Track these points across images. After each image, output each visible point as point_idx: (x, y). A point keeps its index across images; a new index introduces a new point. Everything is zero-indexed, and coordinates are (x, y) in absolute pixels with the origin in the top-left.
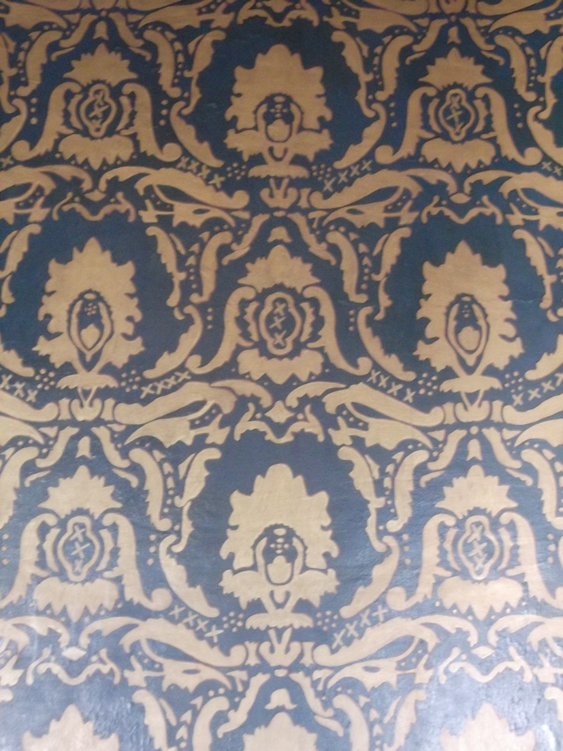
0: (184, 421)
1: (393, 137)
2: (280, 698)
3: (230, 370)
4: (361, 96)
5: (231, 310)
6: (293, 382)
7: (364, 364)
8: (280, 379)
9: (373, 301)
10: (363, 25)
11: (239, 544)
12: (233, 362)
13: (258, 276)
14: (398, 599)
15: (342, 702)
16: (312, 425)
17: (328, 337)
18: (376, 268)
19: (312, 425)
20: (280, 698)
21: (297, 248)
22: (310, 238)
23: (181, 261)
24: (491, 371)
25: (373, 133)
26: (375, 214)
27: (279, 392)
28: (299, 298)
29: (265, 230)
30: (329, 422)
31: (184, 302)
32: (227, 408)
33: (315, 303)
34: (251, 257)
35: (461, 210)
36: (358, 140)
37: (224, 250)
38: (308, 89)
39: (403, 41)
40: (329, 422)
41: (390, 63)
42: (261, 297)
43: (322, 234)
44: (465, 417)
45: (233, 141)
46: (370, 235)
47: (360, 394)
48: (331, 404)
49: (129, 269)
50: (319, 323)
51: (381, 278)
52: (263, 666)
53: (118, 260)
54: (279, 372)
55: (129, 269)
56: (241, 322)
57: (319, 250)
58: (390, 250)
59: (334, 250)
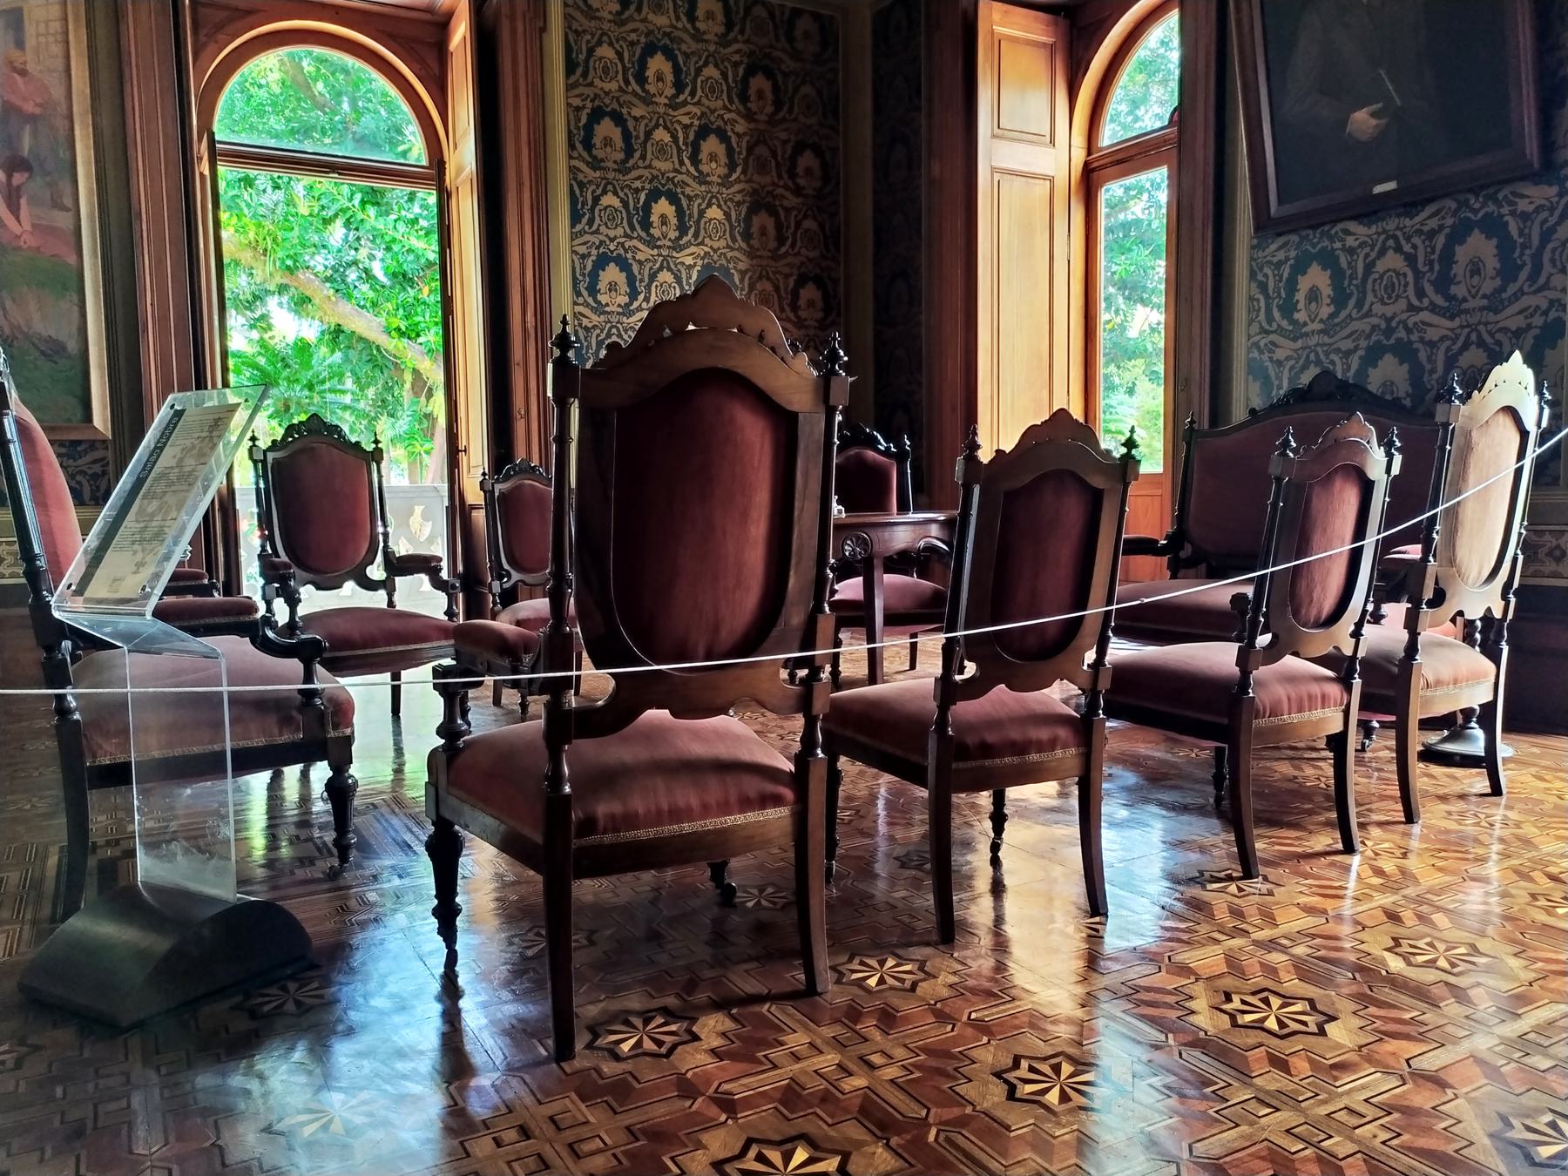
0: (1521, 317)
5: (1547, 256)
7: (1426, 301)
8: (1389, 315)
9: (1431, 269)
12: (1370, 310)
17: (1411, 291)
18: (1433, 252)
22: (1403, 242)
23: (1521, 234)
24: (1321, 321)
28: (1398, 274)
31: (1522, 254)
32: (1544, 306)
35: (1314, 246)
37: (1367, 255)
38: (621, 278)
42: (1381, 277)
43: (1408, 239)
44: (1471, 321)
48: (1410, 323)
49: (1494, 241)
50: (1406, 284)
51: (1435, 257)
52: (1385, 231)
53: (1489, 237)
55: (1494, 241)
56: (1374, 291)
58: (1440, 240)
59: (1415, 247)
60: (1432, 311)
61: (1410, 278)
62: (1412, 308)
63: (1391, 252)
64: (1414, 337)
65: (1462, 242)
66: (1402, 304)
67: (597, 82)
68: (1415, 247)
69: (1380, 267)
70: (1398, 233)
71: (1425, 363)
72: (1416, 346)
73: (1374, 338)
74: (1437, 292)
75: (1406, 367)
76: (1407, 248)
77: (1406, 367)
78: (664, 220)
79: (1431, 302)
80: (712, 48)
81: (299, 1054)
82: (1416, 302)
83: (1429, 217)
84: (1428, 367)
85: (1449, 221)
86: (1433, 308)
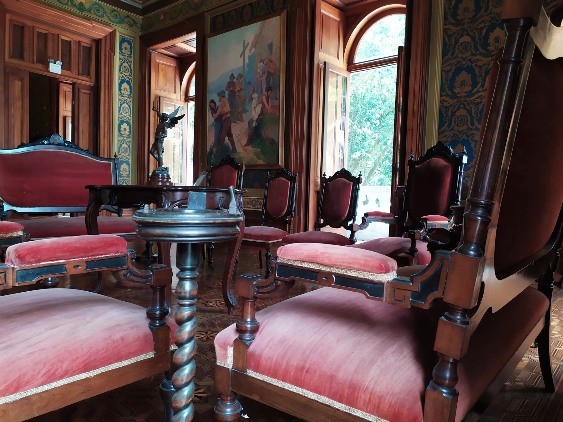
1: (486, 10)
2: (462, 106)
3: (452, 129)
4: (473, 153)
6: (463, 131)
7: (474, 127)
9: (477, 116)
10: (478, 65)
11: (457, 84)
12: (457, 55)
13: (461, 40)
14: (481, 89)
15: (471, 105)
16: (469, 64)
17: (469, 122)
19: (469, 64)
20: (462, 106)
21: (465, 108)
22: (467, 106)
25: (479, 85)
26: (478, 100)
27: (464, 59)
28: (464, 116)
29: (459, 105)
30: (472, 63)
31: (449, 47)
33: (467, 117)
34: (457, 110)
36: (476, 87)
39: (486, 67)
40: (472, 63)
41: (483, 71)
43: (468, 105)
45: (455, 90)
46: (477, 104)
47: (477, 57)
48: (468, 133)
50: (467, 120)
52: (459, 102)
54: (464, 56)
56: (458, 49)
57: (468, 108)
59: (471, 108)
60: (481, 55)
61: (469, 118)
62: (473, 55)
63: (465, 35)
64: (473, 65)
65: (492, 31)
66: (469, 53)
67: (122, 154)
68: (474, 33)
69: (458, 113)
70: (468, 29)
71: (473, 147)
72: (470, 141)
73: (458, 66)
74: (482, 49)
75: (470, 75)
76: (471, 34)
77: (470, 75)
78: (125, 129)
79: (480, 52)
80: (126, 98)
81: (367, 338)
82: (470, 126)
83: (480, 23)
84: (478, 75)
85: (488, 24)
86: (481, 54)
